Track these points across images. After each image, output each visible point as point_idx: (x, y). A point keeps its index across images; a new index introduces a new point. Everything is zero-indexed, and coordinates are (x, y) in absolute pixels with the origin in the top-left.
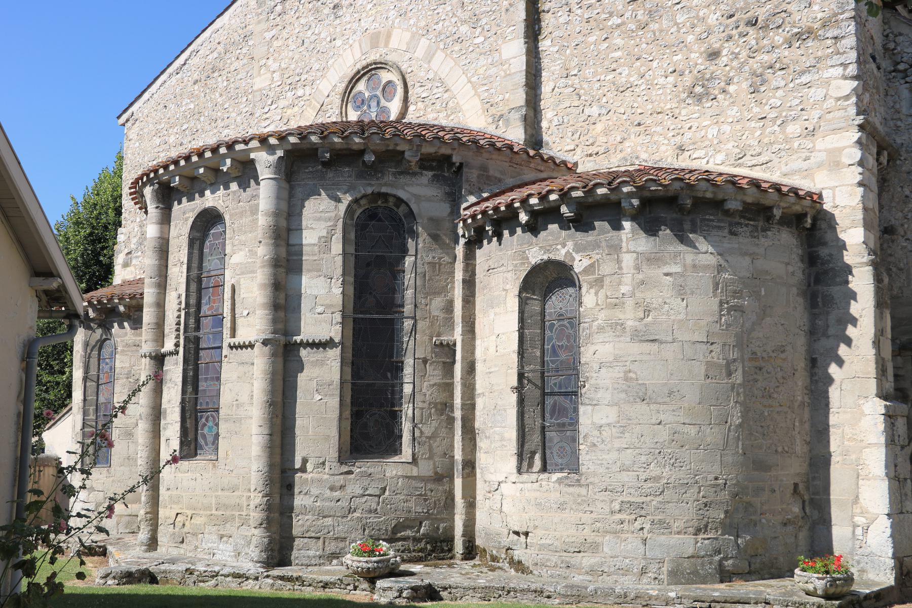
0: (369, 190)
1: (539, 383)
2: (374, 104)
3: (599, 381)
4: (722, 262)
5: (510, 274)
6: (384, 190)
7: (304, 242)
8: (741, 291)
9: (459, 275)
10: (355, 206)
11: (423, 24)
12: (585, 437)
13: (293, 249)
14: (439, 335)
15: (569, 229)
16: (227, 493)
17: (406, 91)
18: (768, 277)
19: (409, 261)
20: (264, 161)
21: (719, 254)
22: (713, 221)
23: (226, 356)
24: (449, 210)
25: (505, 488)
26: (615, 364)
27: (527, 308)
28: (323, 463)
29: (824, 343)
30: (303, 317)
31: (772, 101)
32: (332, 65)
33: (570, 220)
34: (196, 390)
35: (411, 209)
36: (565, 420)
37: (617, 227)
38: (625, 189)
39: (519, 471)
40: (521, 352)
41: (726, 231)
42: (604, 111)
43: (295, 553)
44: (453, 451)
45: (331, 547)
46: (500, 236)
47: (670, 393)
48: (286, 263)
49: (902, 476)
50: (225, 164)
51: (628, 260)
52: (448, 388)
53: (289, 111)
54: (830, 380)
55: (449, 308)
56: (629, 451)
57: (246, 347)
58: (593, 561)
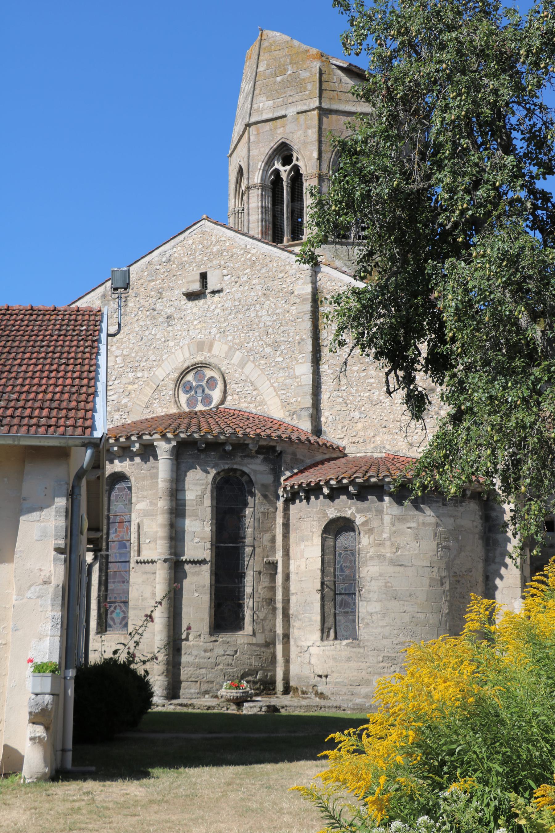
0: (227, 467)
1: (333, 587)
2: (200, 391)
4: (439, 522)
6: (235, 467)
7: (187, 498)
8: (448, 537)
9: (280, 520)
10: (217, 476)
11: (237, 341)
13: (180, 502)
14: (267, 557)
15: (353, 499)
17: (225, 386)
19: (248, 511)
20: (163, 449)
21: (437, 517)
23: (133, 568)
24: (273, 479)
25: (313, 650)
27: (326, 543)
28: (200, 635)
29: (493, 567)
30: (186, 545)
32: (166, 359)
33: (353, 494)
34: (106, 589)
35: (251, 479)
36: (348, 609)
37: (381, 500)
38: (387, 480)
39: (322, 639)
40: (323, 570)
41: (441, 503)
42: (363, 416)
43: (182, 691)
44: (275, 628)
45: (205, 687)
46: (308, 499)
47: (410, 595)
48: (177, 511)
50: (134, 447)
51: (387, 519)
52: (273, 589)
53: (130, 387)
54: (496, 588)
55: (273, 540)
56: (388, 628)
57: (148, 562)
58: (367, 690)
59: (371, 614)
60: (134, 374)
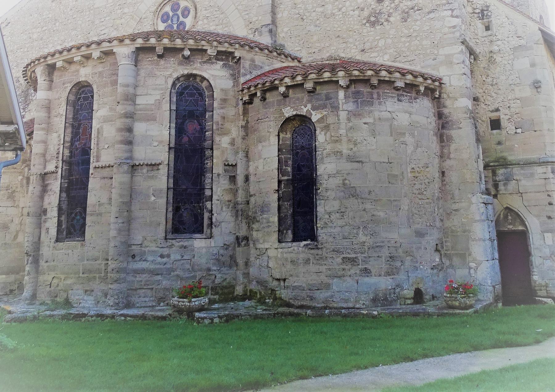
0: (186, 72)
3: (328, 186)
5: (272, 122)
6: (194, 72)
12: (320, 219)
16: (90, 262)
17: (196, 13)
18: (419, 125)
20: (124, 52)
22: (389, 93)
23: (92, 174)
26: (337, 175)
31: (414, 27)
35: (210, 84)
39: (280, 241)
41: (396, 99)
49: (492, 238)
51: (343, 115)
59: (330, 214)
60: (121, 10)
